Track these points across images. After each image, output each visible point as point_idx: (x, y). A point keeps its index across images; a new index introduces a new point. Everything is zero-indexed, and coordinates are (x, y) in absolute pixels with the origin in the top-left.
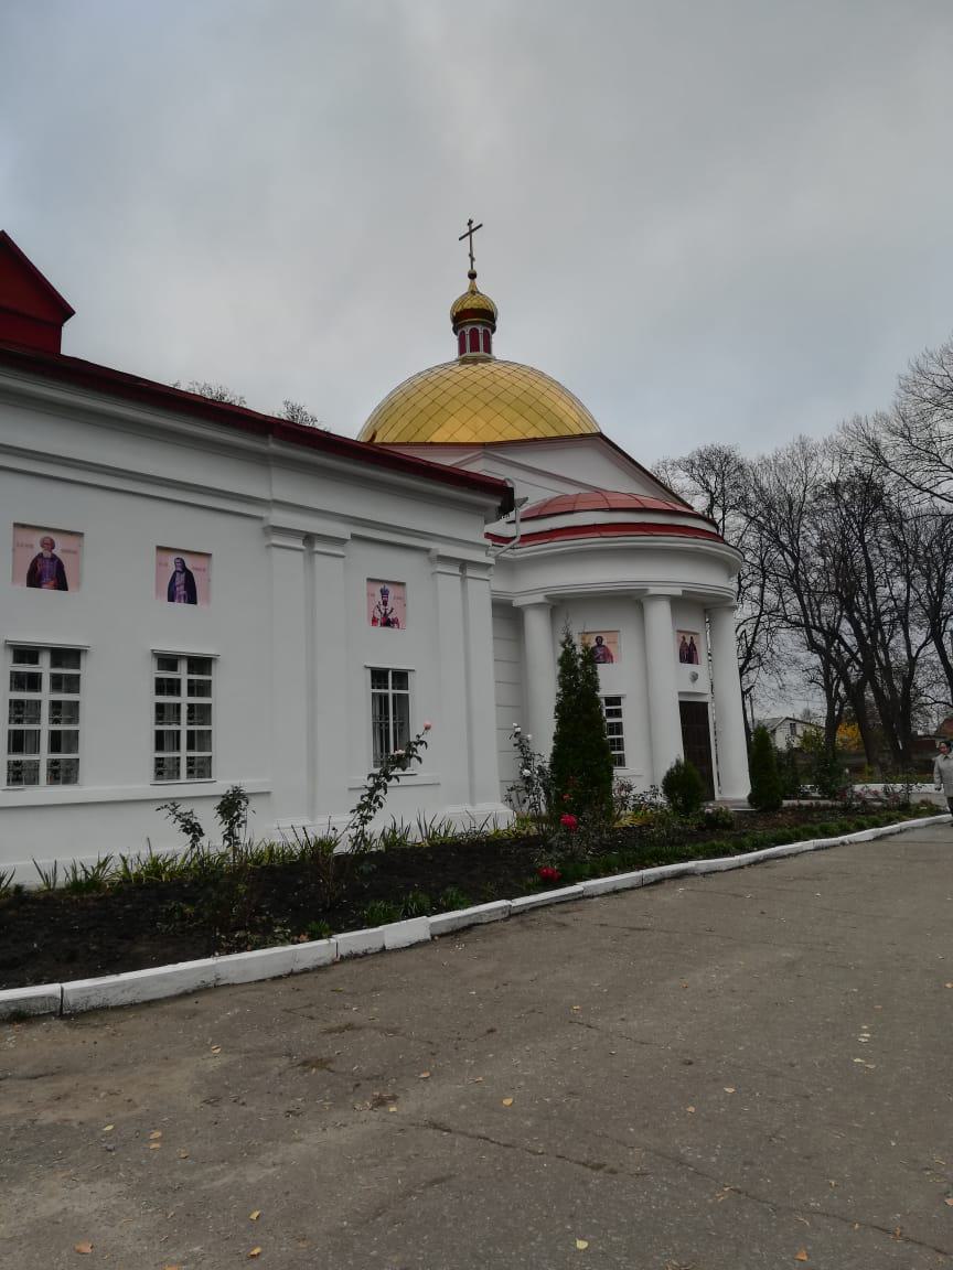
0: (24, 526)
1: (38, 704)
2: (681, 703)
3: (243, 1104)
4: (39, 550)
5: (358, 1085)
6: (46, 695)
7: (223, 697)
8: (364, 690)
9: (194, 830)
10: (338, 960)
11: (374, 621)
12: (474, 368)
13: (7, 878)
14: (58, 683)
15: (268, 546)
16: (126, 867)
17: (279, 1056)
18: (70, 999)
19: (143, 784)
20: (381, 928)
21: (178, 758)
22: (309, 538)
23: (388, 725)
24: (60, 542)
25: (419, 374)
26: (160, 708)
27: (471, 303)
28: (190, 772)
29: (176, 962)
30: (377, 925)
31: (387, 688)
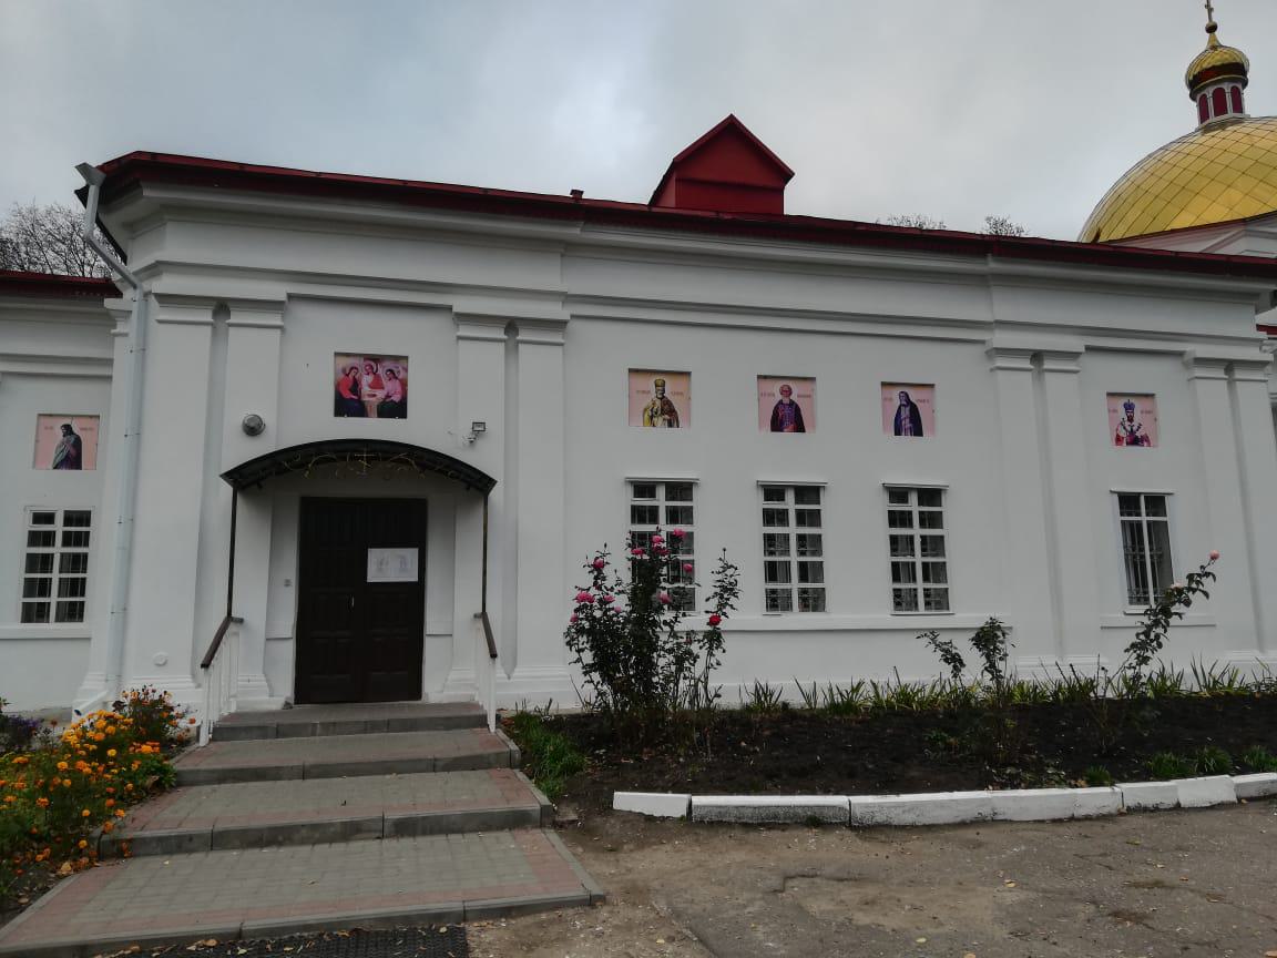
0: (765, 377)
1: (786, 537)
3: (1055, 944)
4: (779, 397)
5: (1186, 949)
6: (793, 530)
7: (955, 528)
8: (1110, 522)
9: (955, 661)
10: (1124, 810)
11: (1119, 440)
12: (1222, 134)
13: (776, 695)
14: (802, 518)
15: (992, 370)
16: (877, 693)
17: (1083, 901)
18: (858, 812)
19: (885, 615)
20: (1173, 783)
21: (915, 590)
22: (1037, 356)
23: (1143, 557)
24: (671, 386)
25: (1150, 156)
26: (894, 540)
27: (1216, 59)
28: (927, 604)
29: (951, 790)
30: (1167, 779)
31: (1139, 515)
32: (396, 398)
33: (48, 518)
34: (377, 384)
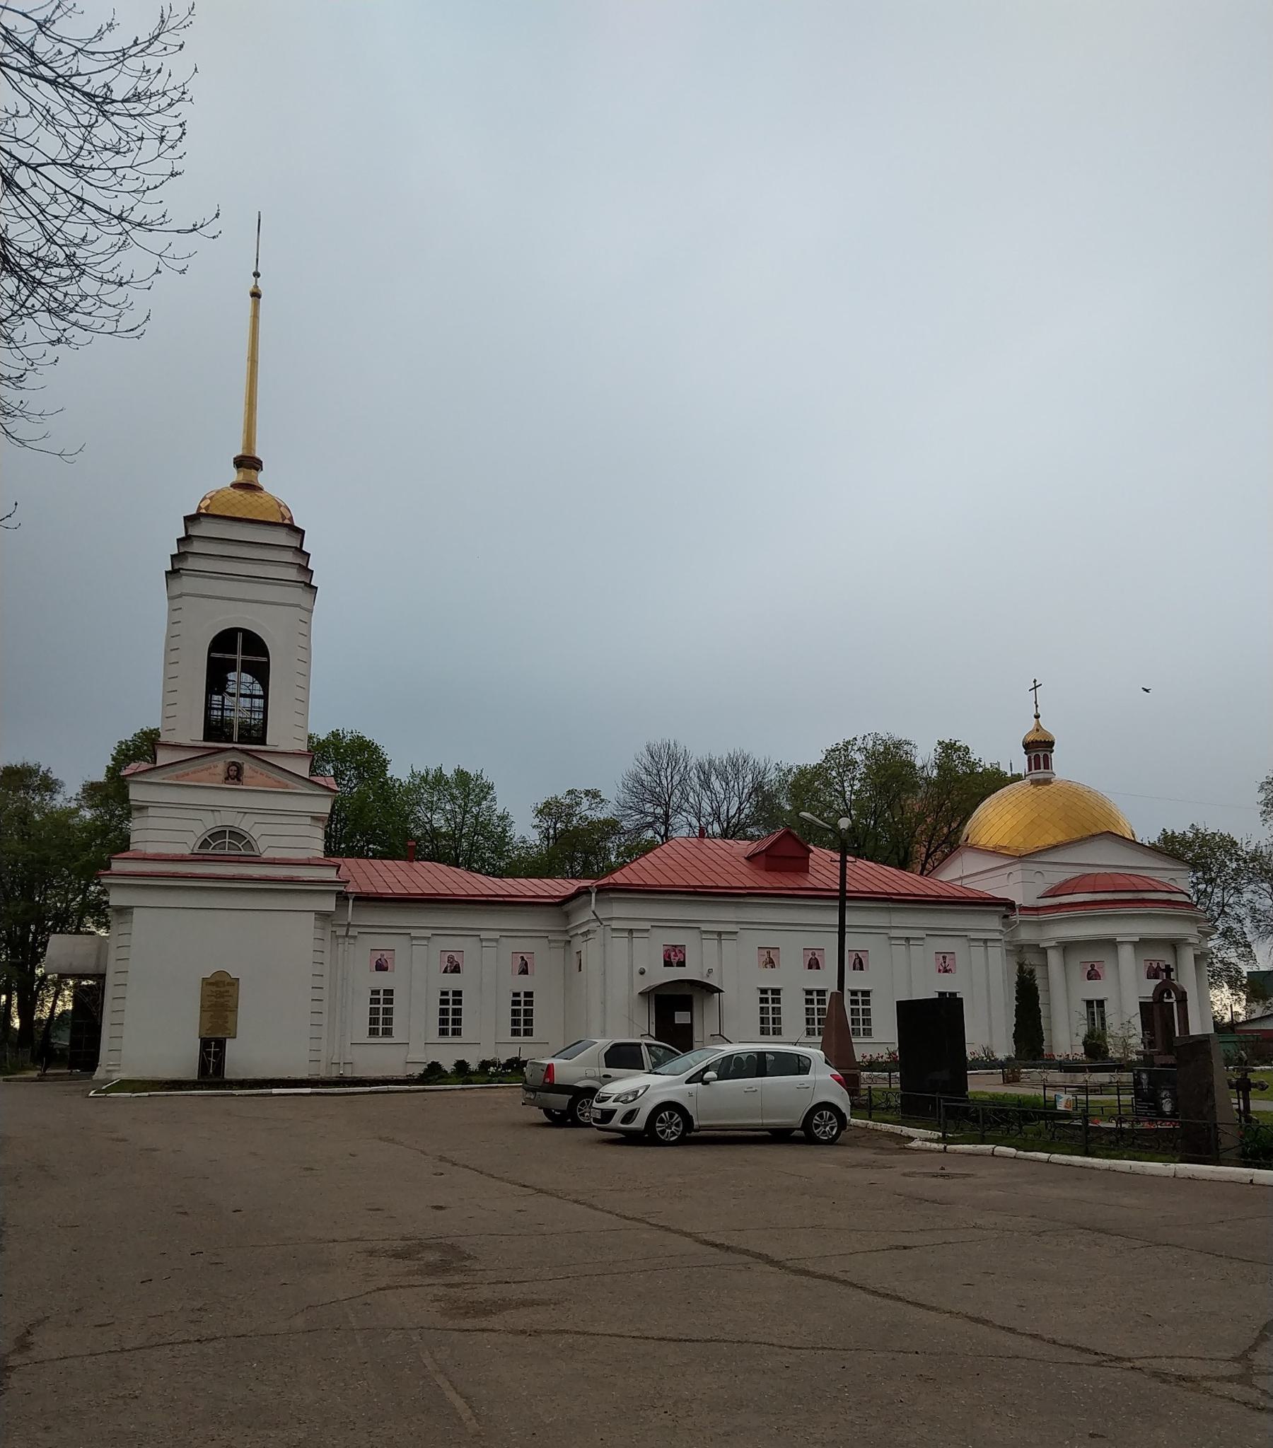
2: (1140, 1003)
6: (451, 1007)
11: (940, 971)
26: (807, 1009)
28: (864, 1034)
32: (682, 960)
33: (377, 992)
34: (676, 955)
